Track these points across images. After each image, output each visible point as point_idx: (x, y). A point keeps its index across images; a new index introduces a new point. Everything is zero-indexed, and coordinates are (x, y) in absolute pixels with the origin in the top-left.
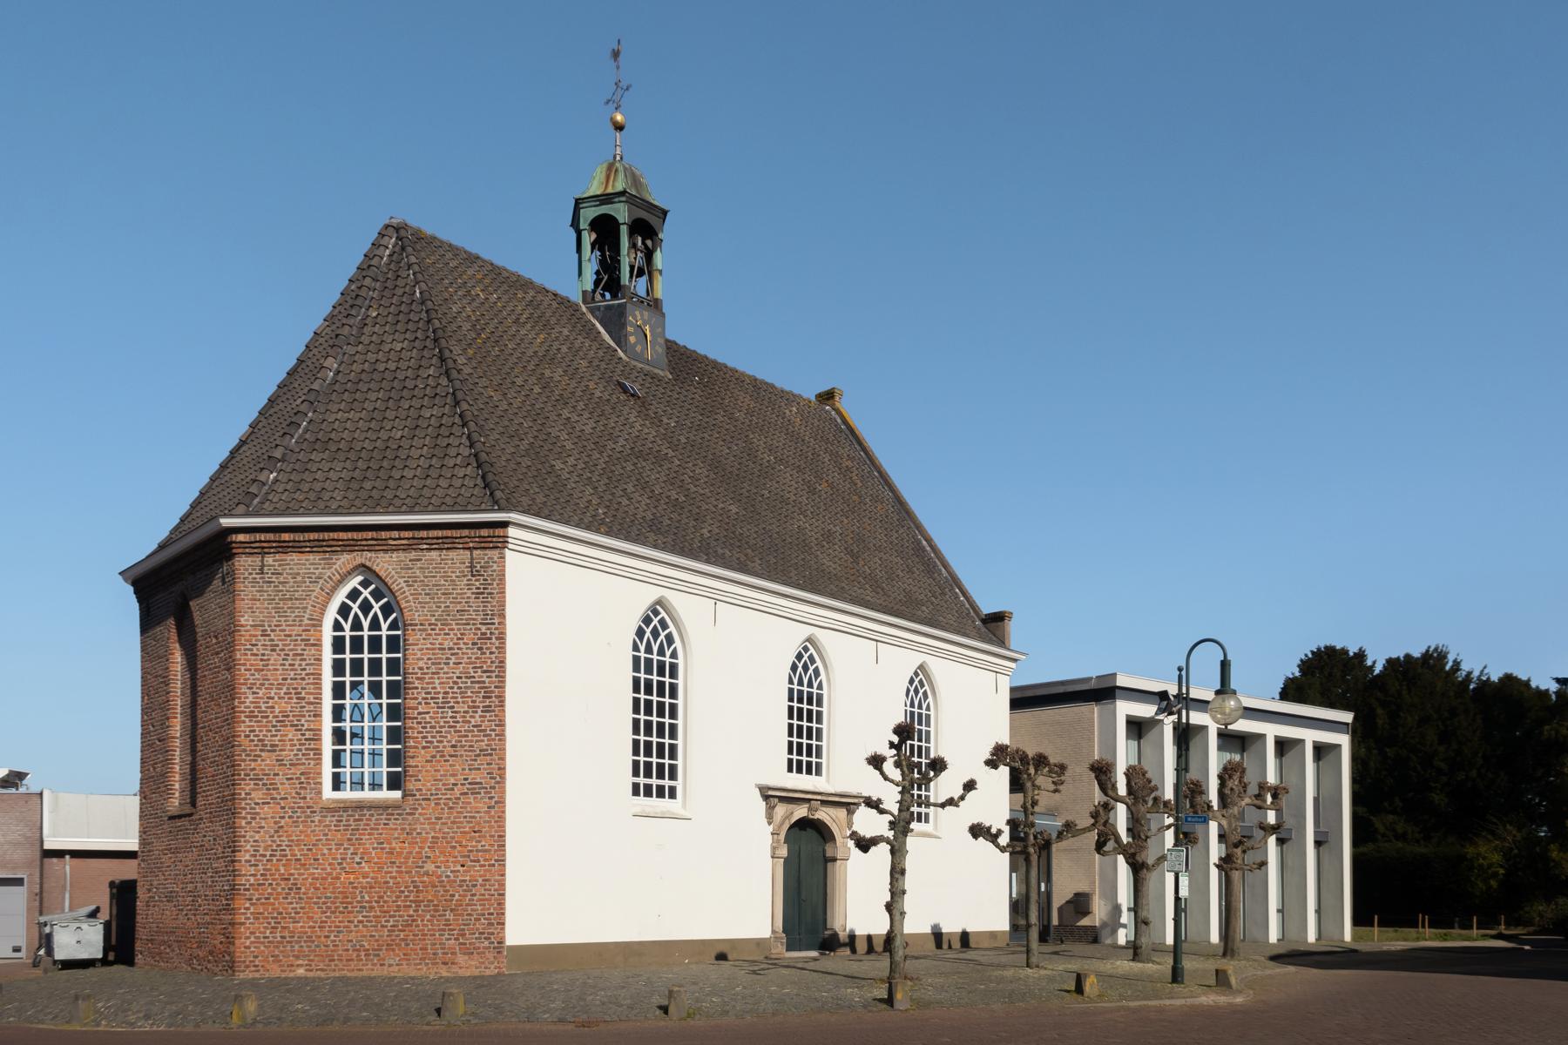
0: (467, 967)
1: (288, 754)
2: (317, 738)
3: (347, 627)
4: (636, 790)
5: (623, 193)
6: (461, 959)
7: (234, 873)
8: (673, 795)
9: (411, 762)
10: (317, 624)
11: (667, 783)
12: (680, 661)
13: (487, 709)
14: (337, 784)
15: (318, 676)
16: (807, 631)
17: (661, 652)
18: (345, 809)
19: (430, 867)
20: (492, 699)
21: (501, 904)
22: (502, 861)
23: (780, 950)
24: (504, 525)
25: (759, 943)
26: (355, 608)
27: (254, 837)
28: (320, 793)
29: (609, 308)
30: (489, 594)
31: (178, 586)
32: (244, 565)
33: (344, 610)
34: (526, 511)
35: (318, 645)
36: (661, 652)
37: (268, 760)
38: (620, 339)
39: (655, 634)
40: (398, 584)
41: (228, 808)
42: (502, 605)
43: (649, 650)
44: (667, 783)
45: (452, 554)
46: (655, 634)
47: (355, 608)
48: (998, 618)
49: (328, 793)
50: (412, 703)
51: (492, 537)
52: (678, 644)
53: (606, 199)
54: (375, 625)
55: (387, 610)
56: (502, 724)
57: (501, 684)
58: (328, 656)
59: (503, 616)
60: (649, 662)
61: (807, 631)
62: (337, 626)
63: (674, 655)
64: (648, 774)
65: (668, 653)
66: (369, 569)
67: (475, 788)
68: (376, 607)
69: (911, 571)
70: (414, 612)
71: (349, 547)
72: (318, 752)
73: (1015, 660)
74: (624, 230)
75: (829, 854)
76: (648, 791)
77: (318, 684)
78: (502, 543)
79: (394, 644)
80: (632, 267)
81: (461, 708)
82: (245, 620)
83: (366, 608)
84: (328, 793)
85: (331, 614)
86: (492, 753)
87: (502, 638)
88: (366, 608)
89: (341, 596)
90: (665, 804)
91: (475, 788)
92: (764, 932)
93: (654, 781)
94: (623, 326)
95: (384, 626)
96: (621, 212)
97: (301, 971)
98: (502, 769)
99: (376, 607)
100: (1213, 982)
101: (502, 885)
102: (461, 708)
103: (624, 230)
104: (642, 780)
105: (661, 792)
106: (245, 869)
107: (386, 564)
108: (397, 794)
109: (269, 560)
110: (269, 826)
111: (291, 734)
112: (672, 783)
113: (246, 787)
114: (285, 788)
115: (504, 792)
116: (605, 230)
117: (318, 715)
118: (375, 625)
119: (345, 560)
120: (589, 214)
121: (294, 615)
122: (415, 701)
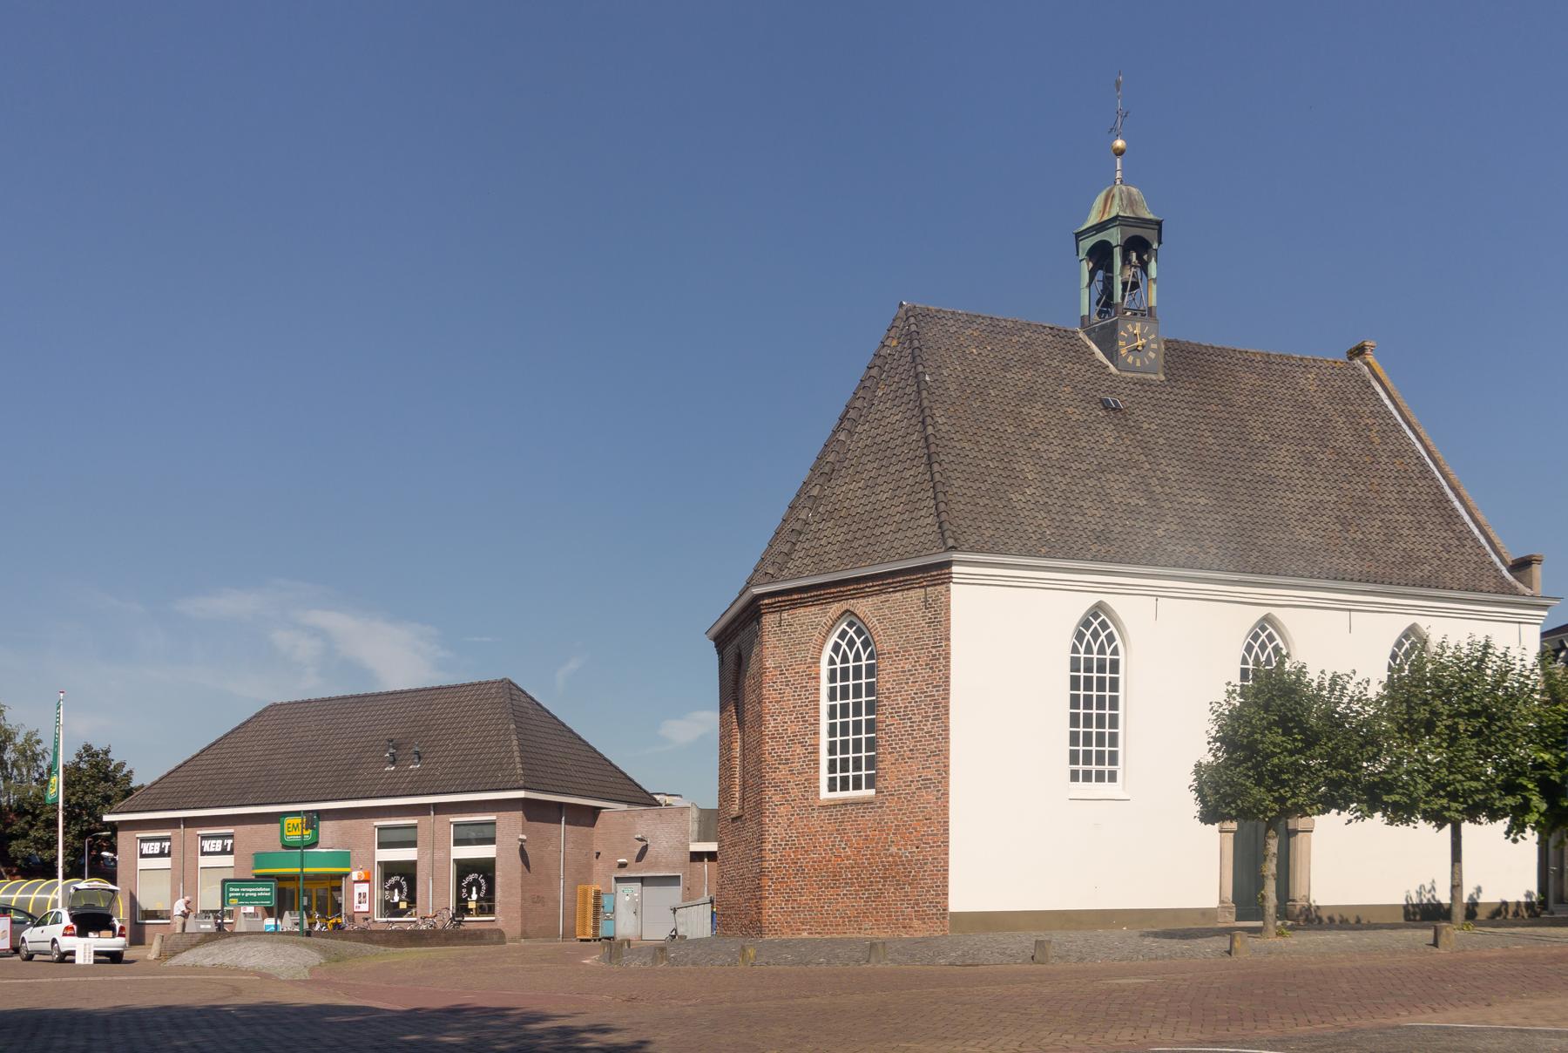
0: (920, 930)
1: (797, 766)
2: (816, 752)
3: (838, 661)
4: (1074, 776)
5: (1116, 217)
6: (916, 923)
7: (762, 859)
8: (1113, 777)
9: (881, 766)
10: (817, 661)
11: (1107, 768)
12: (1121, 657)
13: (936, 718)
14: (832, 788)
15: (817, 703)
16: (1264, 611)
17: (1102, 650)
18: (835, 806)
19: (894, 849)
20: (940, 709)
21: (945, 878)
22: (946, 843)
23: (1230, 920)
24: (949, 564)
25: (1204, 913)
26: (844, 645)
27: (775, 831)
28: (818, 794)
29: (1102, 327)
30: (939, 619)
31: (736, 640)
32: (769, 620)
33: (836, 648)
34: (972, 550)
35: (817, 678)
36: (1102, 650)
37: (784, 770)
38: (1112, 354)
39: (1095, 635)
40: (873, 622)
41: (759, 808)
42: (948, 630)
43: (1089, 650)
44: (1107, 768)
45: (911, 593)
46: (1095, 635)
47: (844, 645)
48: (1522, 566)
49: (825, 794)
50: (881, 718)
51: (938, 574)
52: (1118, 641)
53: (1101, 227)
54: (857, 657)
55: (866, 644)
56: (947, 729)
57: (946, 698)
58: (825, 685)
59: (948, 639)
60: (1088, 661)
61: (1261, 612)
62: (832, 662)
63: (1115, 651)
64: (1087, 761)
65: (1108, 651)
66: (853, 613)
67: (926, 784)
68: (858, 642)
69: (1421, 526)
70: (884, 644)
71: (838, 598)
72: (817, 762)
73: (1544, 607)
74: (1117, 252)
75: (1291, 827)
76: (1087, 777)
77: (817, 710)
78: (948, 580)
79: (871, 671)
80: (1125, 284)
81: (917, 718)
82: (769, 663)
83: (851, 643)
84: (825, 794)
85: (827, 651)
86: (940, 755)
87: (947, 658)
88: (851, 643)
89: (834, 638)
90: (1104, 789)
91: (926, 784)
92: (1212, 902)
93: (1094, 767)
94: (1115, 342)
95: (864, 657)
96: (1115, 236)
97: (805, 934)
98: (947, 766)
99: (858, 642)
100: (1402, 920)
101: (946, 862)
102: (917, 718)
103: (1117, 252)
104: (1081, 767)
105: (1100, 777)
106: (769, 856)
107: (864, 607)
108: (872, 792)
109: (785, 615)
110: (784, 822)
111: (799, 750)
112: (1113, 768)
113: (770, 792)
114: (795, 792)
115: (947, 785)
116: (1101, 256)
117: (817, 733)
118: (857, 657)
119: (835, 608)
120: (1087, 244)
121: (809, 658)
122: (885, 717)
